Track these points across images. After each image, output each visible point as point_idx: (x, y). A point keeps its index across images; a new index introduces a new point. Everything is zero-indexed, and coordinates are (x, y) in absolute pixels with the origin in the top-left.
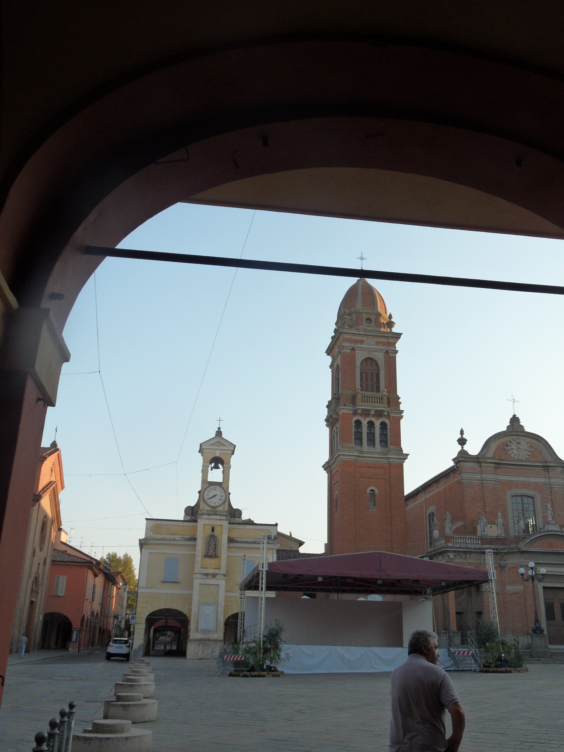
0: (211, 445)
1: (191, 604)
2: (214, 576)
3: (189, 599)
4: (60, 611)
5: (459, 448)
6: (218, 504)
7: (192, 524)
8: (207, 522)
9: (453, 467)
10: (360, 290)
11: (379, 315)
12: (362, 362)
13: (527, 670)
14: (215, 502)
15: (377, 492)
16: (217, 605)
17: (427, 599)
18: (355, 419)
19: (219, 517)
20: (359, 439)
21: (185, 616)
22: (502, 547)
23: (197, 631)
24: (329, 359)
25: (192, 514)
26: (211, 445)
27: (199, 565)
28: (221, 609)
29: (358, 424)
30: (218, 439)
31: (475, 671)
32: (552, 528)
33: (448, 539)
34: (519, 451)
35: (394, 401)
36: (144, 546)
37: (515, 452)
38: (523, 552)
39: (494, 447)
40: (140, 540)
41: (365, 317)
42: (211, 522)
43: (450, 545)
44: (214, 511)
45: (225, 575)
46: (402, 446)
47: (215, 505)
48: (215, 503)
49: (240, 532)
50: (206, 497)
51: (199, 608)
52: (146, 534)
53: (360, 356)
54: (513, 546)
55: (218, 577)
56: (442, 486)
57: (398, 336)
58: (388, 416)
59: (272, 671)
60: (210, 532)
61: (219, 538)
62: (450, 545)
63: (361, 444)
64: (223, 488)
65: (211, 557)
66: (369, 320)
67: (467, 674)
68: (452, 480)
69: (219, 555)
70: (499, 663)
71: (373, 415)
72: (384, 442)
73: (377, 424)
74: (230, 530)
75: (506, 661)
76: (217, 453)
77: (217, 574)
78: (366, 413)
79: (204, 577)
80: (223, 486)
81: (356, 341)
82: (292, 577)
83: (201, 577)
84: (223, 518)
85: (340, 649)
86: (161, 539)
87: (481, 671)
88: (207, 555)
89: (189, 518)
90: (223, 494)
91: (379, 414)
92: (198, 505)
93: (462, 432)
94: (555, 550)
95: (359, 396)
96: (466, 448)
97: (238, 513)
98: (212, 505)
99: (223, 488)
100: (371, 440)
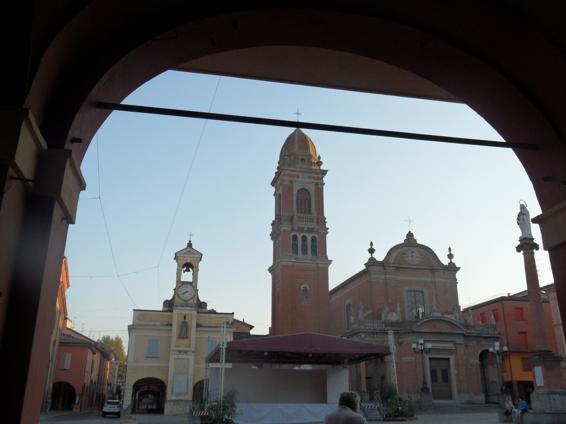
0: (184, 254)
1: (167, 374)
2: (186, 352)
5: (369, 256)
6: (188, 299)
7: (169, 313)
8: (180, 312)
10: (297, 138)
11: (310, 156)
12: (298, 191)
14: (187, 296)
15: (308, 288)
17: (345, 367)
18: (292, 234)
19: (190, 308)
21: (163, 382)
22: (400, 329)
23: (172, 394)
24: (273, 189)
25: (169, 306)
26: (184, 254)
28: (190, 377)
29: (295, 237)
30: (189, 249)
32: (436, 314)
33: (361, 323)
34: (413, 259)
35: (322, 221)
37: (410, 258)
38: (415, 332)
39: (395, 254)
41: (300, 157)
42: (183, 312)
43: (362, 327)
44: (186, 304)
45: (194, 352)
47: (186, 299)
49: (205, 319)
50: (179, 293)
53: (297, 187)
54: (408, 328)
55: (188, 353)
57: (325, 172)
58: (317, 232)
60: (183, 320)
61: (189, 324)
62: (362, 327)
63: (297, 253)
65: (183, 338)
66: (303, 160)
70: (397, 414)
71: (306, 232)
72: (314, 252)
73: (309, 238)
74: (198, 318)
75: (402, 412)
76: (188, 260)
78: (301, 230)
79: (178, 353)
80: (193, 284)
84: (193, 309)
85: (281, 406)
86: (152, 326)
87: (384, 420)
88: (180, 337)
89: (166, 309)
90: (193, 290)
91: (310, 230)
92: (173, 299)
94: (438, 330)
95: (296, 217)
96: (374, 255)
97: (204, 305)
98: (185, 299)
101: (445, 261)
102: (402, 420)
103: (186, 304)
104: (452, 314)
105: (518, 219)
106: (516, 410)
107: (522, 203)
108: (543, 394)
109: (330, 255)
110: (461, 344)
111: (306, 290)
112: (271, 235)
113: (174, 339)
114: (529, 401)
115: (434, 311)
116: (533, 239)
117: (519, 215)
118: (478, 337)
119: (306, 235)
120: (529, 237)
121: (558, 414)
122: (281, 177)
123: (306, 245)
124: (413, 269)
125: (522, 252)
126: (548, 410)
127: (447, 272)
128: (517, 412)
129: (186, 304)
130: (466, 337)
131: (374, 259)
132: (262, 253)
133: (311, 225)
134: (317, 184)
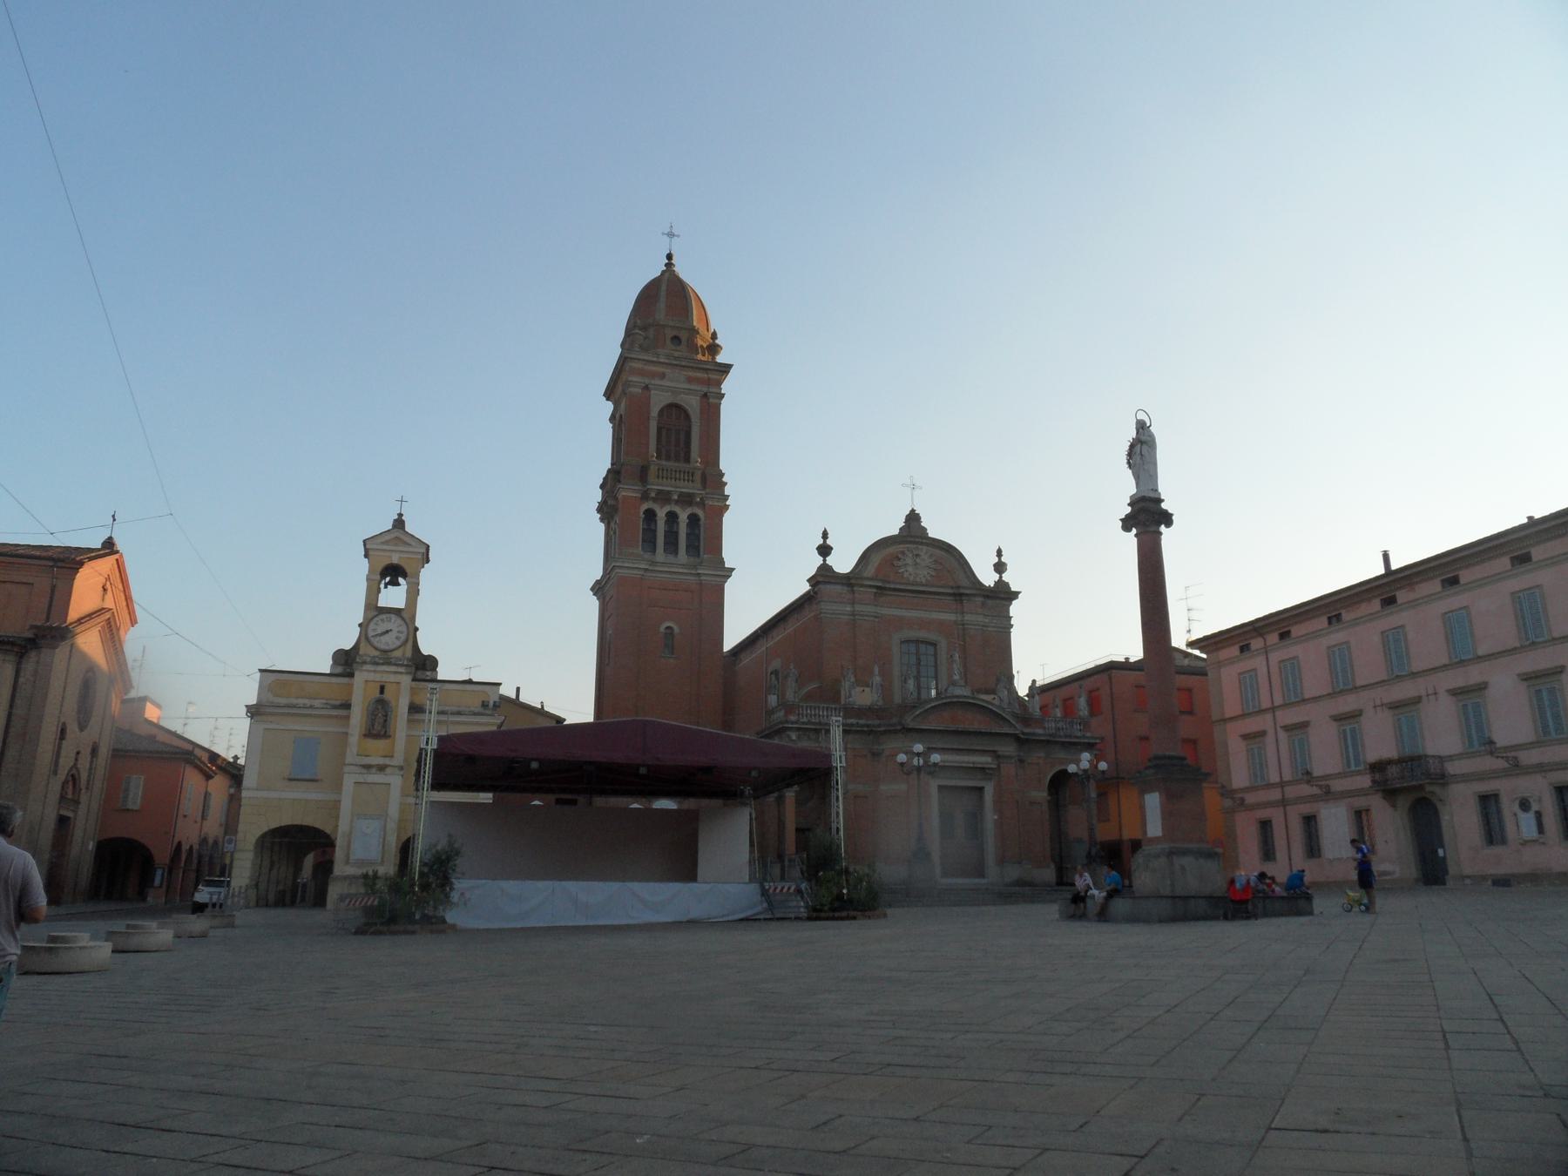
0: (386, 543)
2: (382, 768)
4: (137, 837)
5: (820, 560)
7: (345, 680)
8: (371, 676)
9: (808, 593)
10: (664, 288)
11: (694, 332)
12: (661, 411)
13: (885, 915)
14: (389, 641)
15: (676, 630)
17: (745, 804)
18: (645, 506)
19: (393, 669)
20: (650, 541)
21: (327, 836)
22: (877, 722)
23: (347, 862)
24: (610, 406)
26: (386, 543)
27: (355, 750)
29: (650, 515)
30: (397, 533)
31: (797, 918)
32: (958, 691)
33: (790, 709)
34: (917, 571)
35: (713, 481)
37: (910, 569)
38: (911, 730)
39: (876, 560)
41: (670, 333)
42: (378, 677)
43: (793, 718)
44: (385, 658)
45: (401, 768)
46: (725, 554)
50: (371, 634)
53: (658, 401)
54: (894, 720)
55: (388, 770)
56: (791, 627)
57: (726, 369)
58: (702, 504)
59: (436, 925)
60: (378, 695)
61: (393, 704)
62: (793, 718)
63: (654, 550)
65: (377, 736)
66: (676, 340)
67: (786, 924)
68: (808, 614)
70: (836, 904)
71: (677, 502)
72: (694, 548)
73: (683, 516)
74: (413, 691)
75: (850, 901)
76: (396, 559)
77: (386, 766)
78: (664, 498)
80: (406, 616)
81: (653, 375)
82: (507, 767)
84: (402, 670)
85: (572, 886)
86: (305, 707)
87: (810, 919)
88: (370, 734)
89: (339, 670)
90: (404, 629)
91: (686, 500)
92: (356, 647)
93: (825, 535)
94: (961, 727)
95: (653, 469)
96: (829, 560)
97: (430, 663)
98: (383, 647)
100: (672, 544)
101: (988, 578)
102: (848, 918)
103: (387, 655)
104: (993, 692)
105: (1130, 454)
106: (1095, 892)
107: (1141, 416)
108: (1157, 856)
109: (729, 557)
110: (1010, 757)
111: (672, 634)
112: (599, 510)
113: (354, 739)
114: (1125, 873)
115: (954, 683)
116: (1160, 501)
117: (1132, 446)
118: (1047, 743)
119: (677, 509)
120: (1152, 495)
121: (1186, 898)
122: (624, 377)
123: (676, 534)
124: (918, 593)
125: (1134, 531)
126: (1167, 892)
127: (990, 602)
128: (1098, 894)
129: (387, 655)
130: (1020, 741)
131: (829, 568)
132: (578, 550)
133: (693, 488)
134: (705, 395)
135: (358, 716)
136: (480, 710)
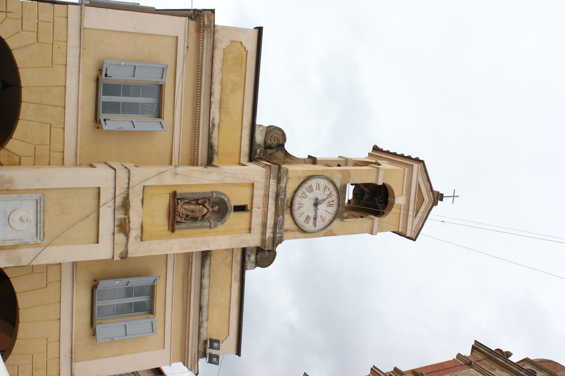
2: (123, 227)
3: (53, 158)
6: (296, 213)
7: (245, 148)
16: (36, 245)
19: (270, 222)
25: (267, 147)
28: (26, 256)
36: (193, 23)
40: (213, 11)
42: (258, 201)
44: (284, 205)
47: (296, 207)
48: (301, 206)
49: (222, 274)
51: (29, 191)
52: (224, 28)
55: (120, 237)
60: (234, 202)
61: (221, 227)
64: (331, 222)
69: (177, 232)
79: (119, 200)
83: (120, 191)
88: (175, 198)
98: (297, 200)
99: (331, 222)
135: (197, 179)
136: (203, 337)
